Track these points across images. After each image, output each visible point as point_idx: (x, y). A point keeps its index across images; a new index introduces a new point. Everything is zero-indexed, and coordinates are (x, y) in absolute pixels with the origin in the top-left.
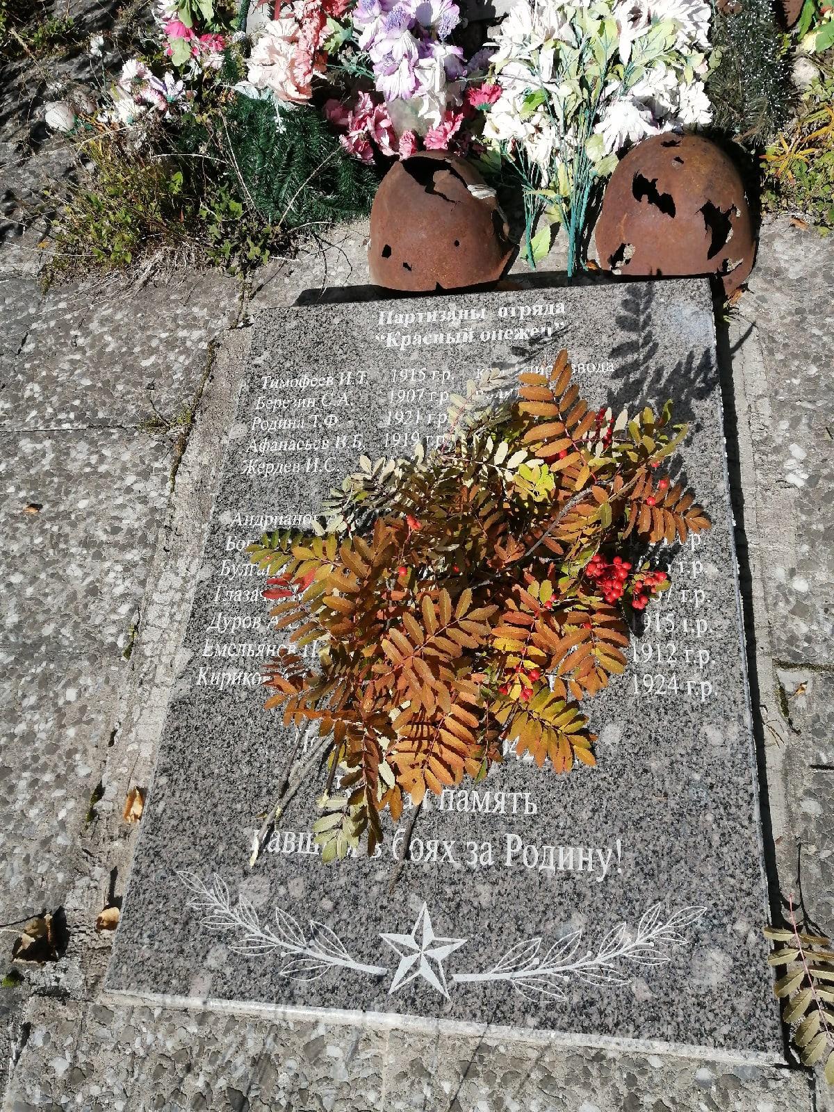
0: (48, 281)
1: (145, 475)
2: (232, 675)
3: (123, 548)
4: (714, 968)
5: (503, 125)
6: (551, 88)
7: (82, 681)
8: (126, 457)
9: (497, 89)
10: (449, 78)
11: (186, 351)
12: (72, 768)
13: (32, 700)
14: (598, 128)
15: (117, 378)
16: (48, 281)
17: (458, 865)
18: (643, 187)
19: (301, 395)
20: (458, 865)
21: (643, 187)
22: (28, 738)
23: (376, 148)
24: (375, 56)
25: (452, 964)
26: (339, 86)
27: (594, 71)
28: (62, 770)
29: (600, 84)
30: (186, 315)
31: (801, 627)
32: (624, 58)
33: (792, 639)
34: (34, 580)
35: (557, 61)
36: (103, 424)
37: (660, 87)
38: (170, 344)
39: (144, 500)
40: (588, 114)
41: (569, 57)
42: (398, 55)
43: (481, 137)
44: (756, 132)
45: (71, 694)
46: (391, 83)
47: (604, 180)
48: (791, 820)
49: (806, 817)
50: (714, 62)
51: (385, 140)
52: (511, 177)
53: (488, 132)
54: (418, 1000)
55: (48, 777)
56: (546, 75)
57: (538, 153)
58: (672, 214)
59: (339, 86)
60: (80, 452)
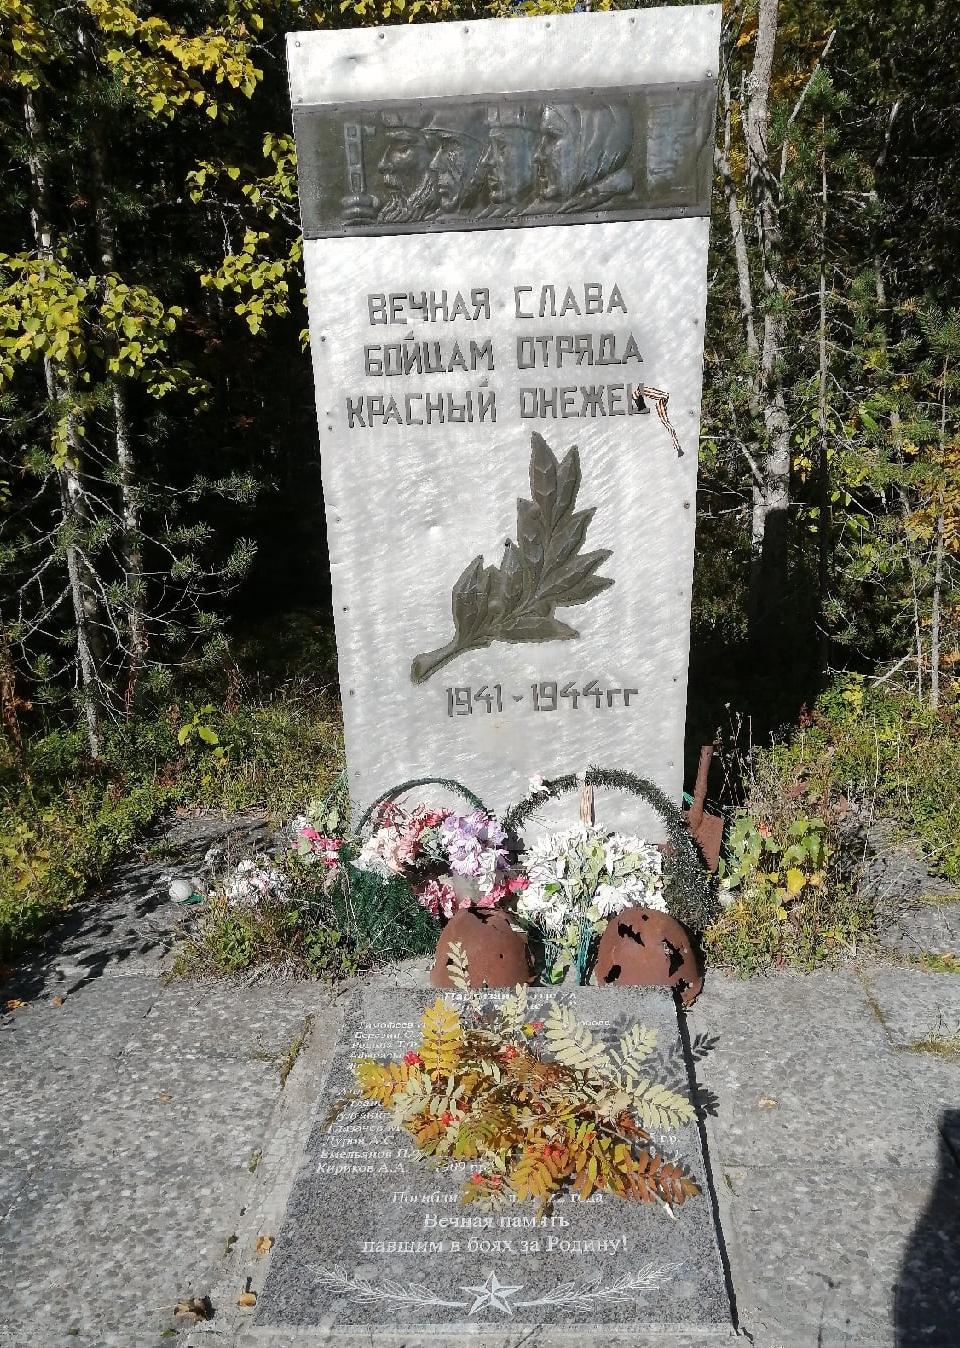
0: (167, 981)
1: (259, 1082)
2: (344, 1168)
3: (243, 1119)
4: (689, 1290)
5: (530, 901)
6: (563, 882)
7: (215, 1185)
8: (242, 1073)
9: (526, 883)
10: (499, 868)
11: (287, 1021)
12: (209, 1228)
13: (174, 1194)
14: (595, 901)
15: (231, 1033)
16: (167, 981)
17: (514, 1252)
18: (624, 930)
19: (387, 1032)
20: (514, 1252)
21: (624, 930)
22: (172, 1214)
23: (441, 909)
24: (451, 850)
25: (518, 1296)
26: (427, 867)
27: (590, 877)
28: (201, 1229)
29: (594, 883)
30: (287, 1001)
31: (739, 1150)
32: (610, 870)
33: (733, 1155)
34: (168, 1135)
35: (566, 869)
36: (221, 1055)
37: (634, 888)
38: (274, 1016)
39: (258, 1095)
40: (584, 897)
41: (575, 864)
42: (468, 847)
43: (515, 909)
44: (695, 916)
45: (206, 1191)
46: (462, 865)
47: (599, 938)
48: (736, 1235)
49: (745, 1233)
50: (667, 882)
51: (449, 905)
52: (536, 933)
53: (520, 905)
54: (490, 1315)
55: (189, 1233)
56: (560, 874)
57: (553, 921)
58: (610, 552)
59: (427, 867)
60: (202, 1071)
